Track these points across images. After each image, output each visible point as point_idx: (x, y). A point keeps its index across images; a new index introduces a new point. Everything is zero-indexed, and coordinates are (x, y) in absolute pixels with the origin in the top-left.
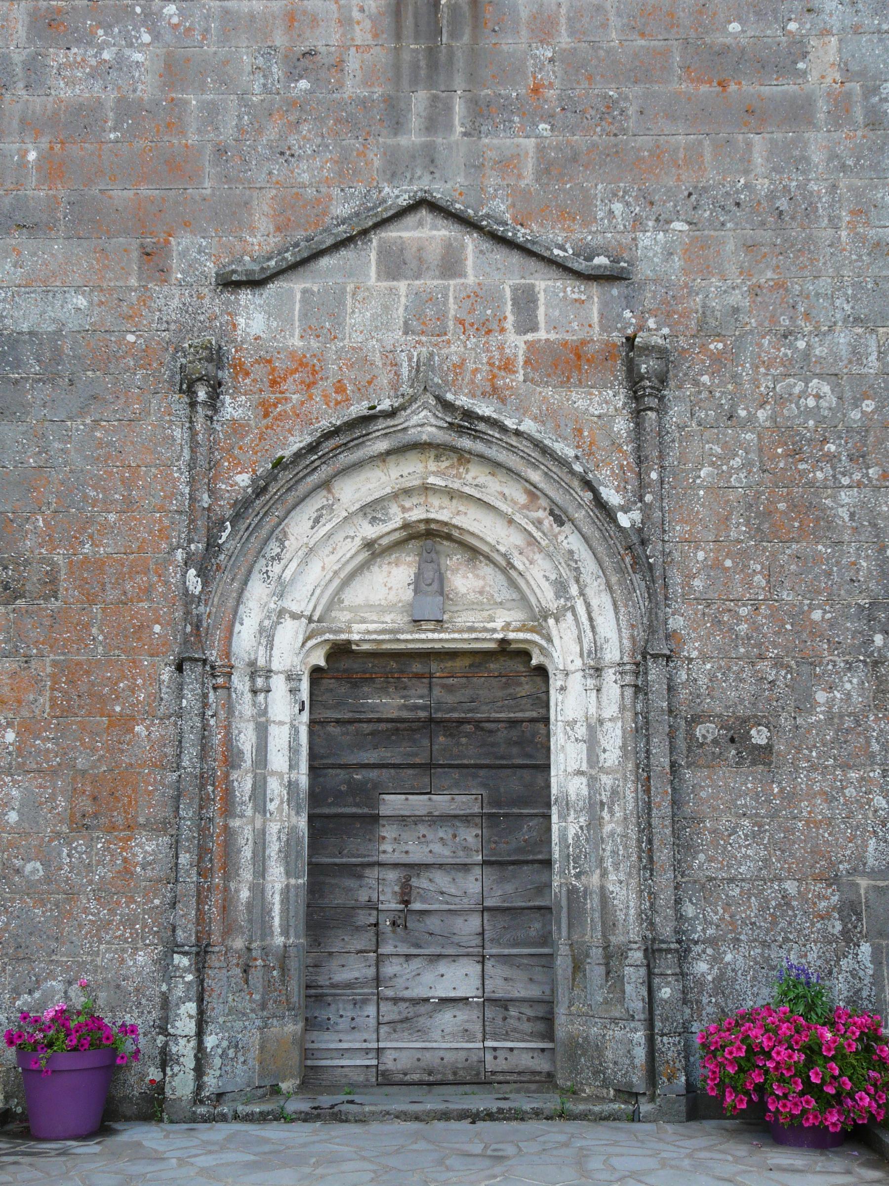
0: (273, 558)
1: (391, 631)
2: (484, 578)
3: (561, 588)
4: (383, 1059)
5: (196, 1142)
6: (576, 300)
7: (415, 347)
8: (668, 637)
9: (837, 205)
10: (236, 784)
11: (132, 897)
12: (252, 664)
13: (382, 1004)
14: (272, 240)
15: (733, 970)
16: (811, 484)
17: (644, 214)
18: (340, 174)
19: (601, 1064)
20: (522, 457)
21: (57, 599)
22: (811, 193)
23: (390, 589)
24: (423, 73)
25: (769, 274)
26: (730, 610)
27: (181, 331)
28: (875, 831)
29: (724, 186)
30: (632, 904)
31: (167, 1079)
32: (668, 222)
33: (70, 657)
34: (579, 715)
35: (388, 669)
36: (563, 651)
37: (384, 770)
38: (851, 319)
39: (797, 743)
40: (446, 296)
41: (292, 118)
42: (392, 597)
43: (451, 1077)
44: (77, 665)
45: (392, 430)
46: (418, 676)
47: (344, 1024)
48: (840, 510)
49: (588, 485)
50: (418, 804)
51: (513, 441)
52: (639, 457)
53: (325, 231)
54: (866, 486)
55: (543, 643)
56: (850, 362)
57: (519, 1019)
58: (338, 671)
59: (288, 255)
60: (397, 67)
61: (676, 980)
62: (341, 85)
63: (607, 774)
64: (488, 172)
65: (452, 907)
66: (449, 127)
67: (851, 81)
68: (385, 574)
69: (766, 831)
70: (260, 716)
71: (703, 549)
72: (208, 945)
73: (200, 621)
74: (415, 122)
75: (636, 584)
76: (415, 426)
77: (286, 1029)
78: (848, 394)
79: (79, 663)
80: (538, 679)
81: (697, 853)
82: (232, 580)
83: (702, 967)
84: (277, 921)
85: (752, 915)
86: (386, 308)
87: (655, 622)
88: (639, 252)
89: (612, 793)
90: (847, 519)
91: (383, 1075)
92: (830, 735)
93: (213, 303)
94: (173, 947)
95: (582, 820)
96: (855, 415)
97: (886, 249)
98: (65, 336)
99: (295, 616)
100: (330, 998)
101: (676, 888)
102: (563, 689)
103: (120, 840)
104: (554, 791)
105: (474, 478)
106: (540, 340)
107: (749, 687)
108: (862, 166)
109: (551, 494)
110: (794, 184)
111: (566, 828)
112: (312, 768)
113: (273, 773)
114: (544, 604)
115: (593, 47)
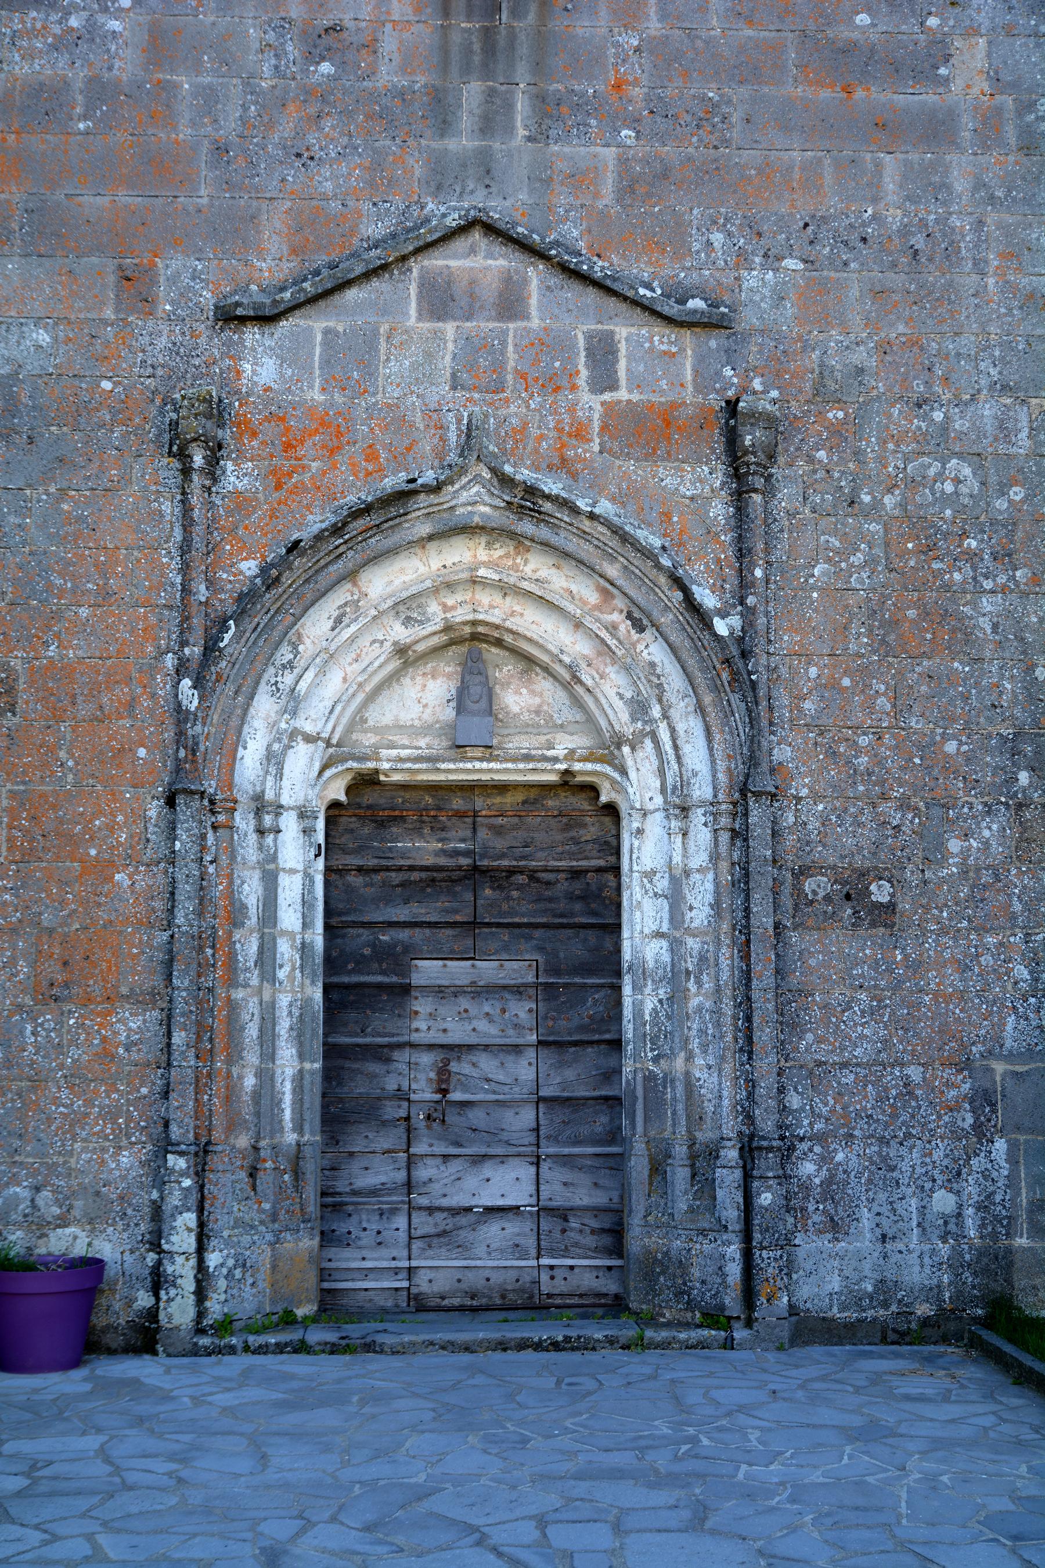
0: (284, 667)
1: (429, 759)
2: (541, 695)
3: (639, 708)
4: (416, 1280)
5: (205, 1379)
6: (665, 353)
7: (465, 406)
8: (772, 771)
9: (984, 246)
10: (238, 946)
11: (114, 1084)
12: (258, 798)
13: (414, 1215)
14: (286, 266)
15: (845, 1172)
16: (947, 587)
17: (749, 248)
18: (372, 184)
19: (685, 1284)
20: (597, 546)
21: (14, 714)
22: (953, 229)
23: (425, 706)
24: (477, 59)
25: (901, 328)
26: (848, 740)
27: (170, 377)
28: (1014, 1007)
29: (847, 217)
30: (725, 1093)
31: (162, 1305)
32: (780, 258)
33: (31, 787)
34: (659, 863)
35: (422, 806)
36: (640, 785)
37: (417, 930)
38: (998, 386)
39: (924, 901)
40: (504, 343)
41: (312, 110)
42: (427, 716)
43: (498, 1302)
44: (40, 796)
45: (436, 509)
46: (460, 815)
47: (368, 1239)
48: (981, 619)
49: (679, 583)
50: (459, 971)
51: (586, 525)
52: (740, 550)
53: (352, 255)
54: (1012, 591)
55: (616, 775)
56: (996, 439)
57: (581, 1231)
58: (359, 806)
59: (306, 285)
60: (444, 50)
61: (779, 1184)
62: (372, 73)
63: (694, 936)
64: (558, 188)
65: (501, 1097)
66: (509, 130)
67: (1002, 93)
68: (418, 688)
69: (886, 1006)
70: (269, 862)
71: (816, 665)
72: (208, 1143)
73: (197, 744)
74: (466, 121)
75: (734, 706)
76: (464, 505)
77: (301, 1244)
78: (993, 479)
79: (43, 795)
80: (607, 820)
81: (804, 1032)
82: (236, 693)
83: (808, 1168)
84: (288, 1114)
85: (869, 1106)
86: (429, 355)
87: (757, 753)
88: (743, 294)
89: (700, 960)
90: (989, 631)
91: (415, 1299)
92: (964, 892)
93: (210, 343)
94: (165, 1146)
95: (661, 992)
96: (1001, 504)
97: (1041, 302)
98: (22, 381)
99: (309, 739)
100: (350, 1208)
101: (779, 1075)
102: (640, 832)
103: (98, 1015)
104: (627, 955)
105: (534, 571)
106: (620, 402)
107: (868, 834)
108: (1014, 199)
109: (632, 593)
110: (933, 217)
111: (642, 1002)
112: (327, 927)
113: (284, 933)
114: (617, 728)
115: (689, 35)
